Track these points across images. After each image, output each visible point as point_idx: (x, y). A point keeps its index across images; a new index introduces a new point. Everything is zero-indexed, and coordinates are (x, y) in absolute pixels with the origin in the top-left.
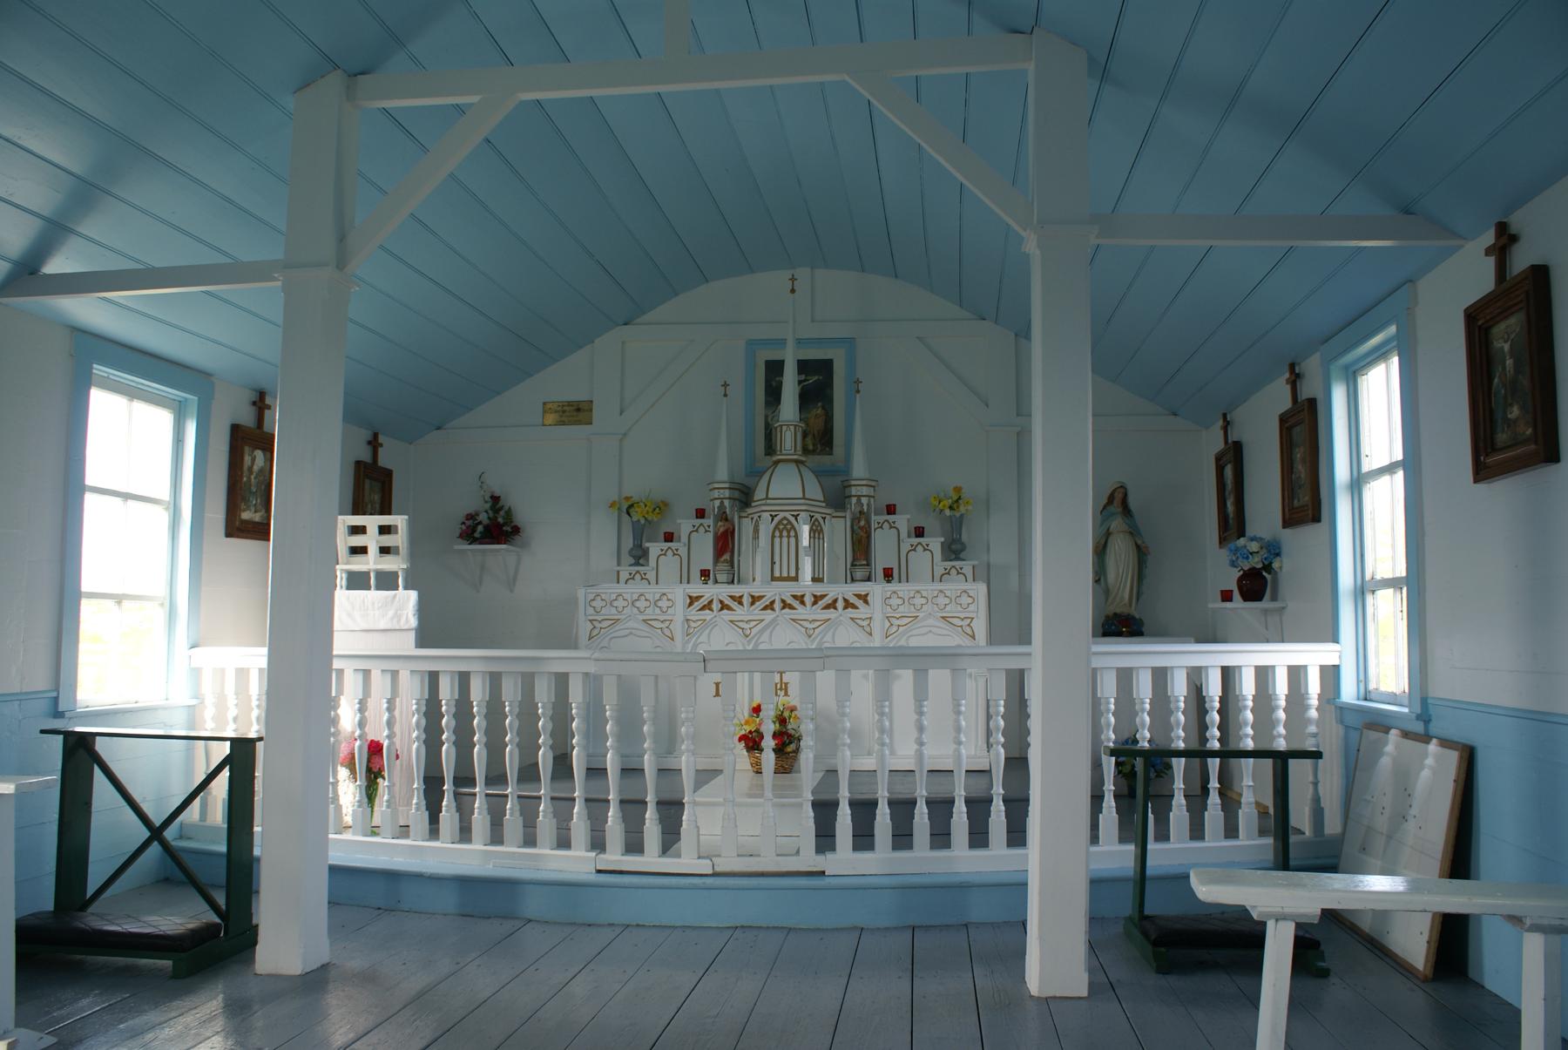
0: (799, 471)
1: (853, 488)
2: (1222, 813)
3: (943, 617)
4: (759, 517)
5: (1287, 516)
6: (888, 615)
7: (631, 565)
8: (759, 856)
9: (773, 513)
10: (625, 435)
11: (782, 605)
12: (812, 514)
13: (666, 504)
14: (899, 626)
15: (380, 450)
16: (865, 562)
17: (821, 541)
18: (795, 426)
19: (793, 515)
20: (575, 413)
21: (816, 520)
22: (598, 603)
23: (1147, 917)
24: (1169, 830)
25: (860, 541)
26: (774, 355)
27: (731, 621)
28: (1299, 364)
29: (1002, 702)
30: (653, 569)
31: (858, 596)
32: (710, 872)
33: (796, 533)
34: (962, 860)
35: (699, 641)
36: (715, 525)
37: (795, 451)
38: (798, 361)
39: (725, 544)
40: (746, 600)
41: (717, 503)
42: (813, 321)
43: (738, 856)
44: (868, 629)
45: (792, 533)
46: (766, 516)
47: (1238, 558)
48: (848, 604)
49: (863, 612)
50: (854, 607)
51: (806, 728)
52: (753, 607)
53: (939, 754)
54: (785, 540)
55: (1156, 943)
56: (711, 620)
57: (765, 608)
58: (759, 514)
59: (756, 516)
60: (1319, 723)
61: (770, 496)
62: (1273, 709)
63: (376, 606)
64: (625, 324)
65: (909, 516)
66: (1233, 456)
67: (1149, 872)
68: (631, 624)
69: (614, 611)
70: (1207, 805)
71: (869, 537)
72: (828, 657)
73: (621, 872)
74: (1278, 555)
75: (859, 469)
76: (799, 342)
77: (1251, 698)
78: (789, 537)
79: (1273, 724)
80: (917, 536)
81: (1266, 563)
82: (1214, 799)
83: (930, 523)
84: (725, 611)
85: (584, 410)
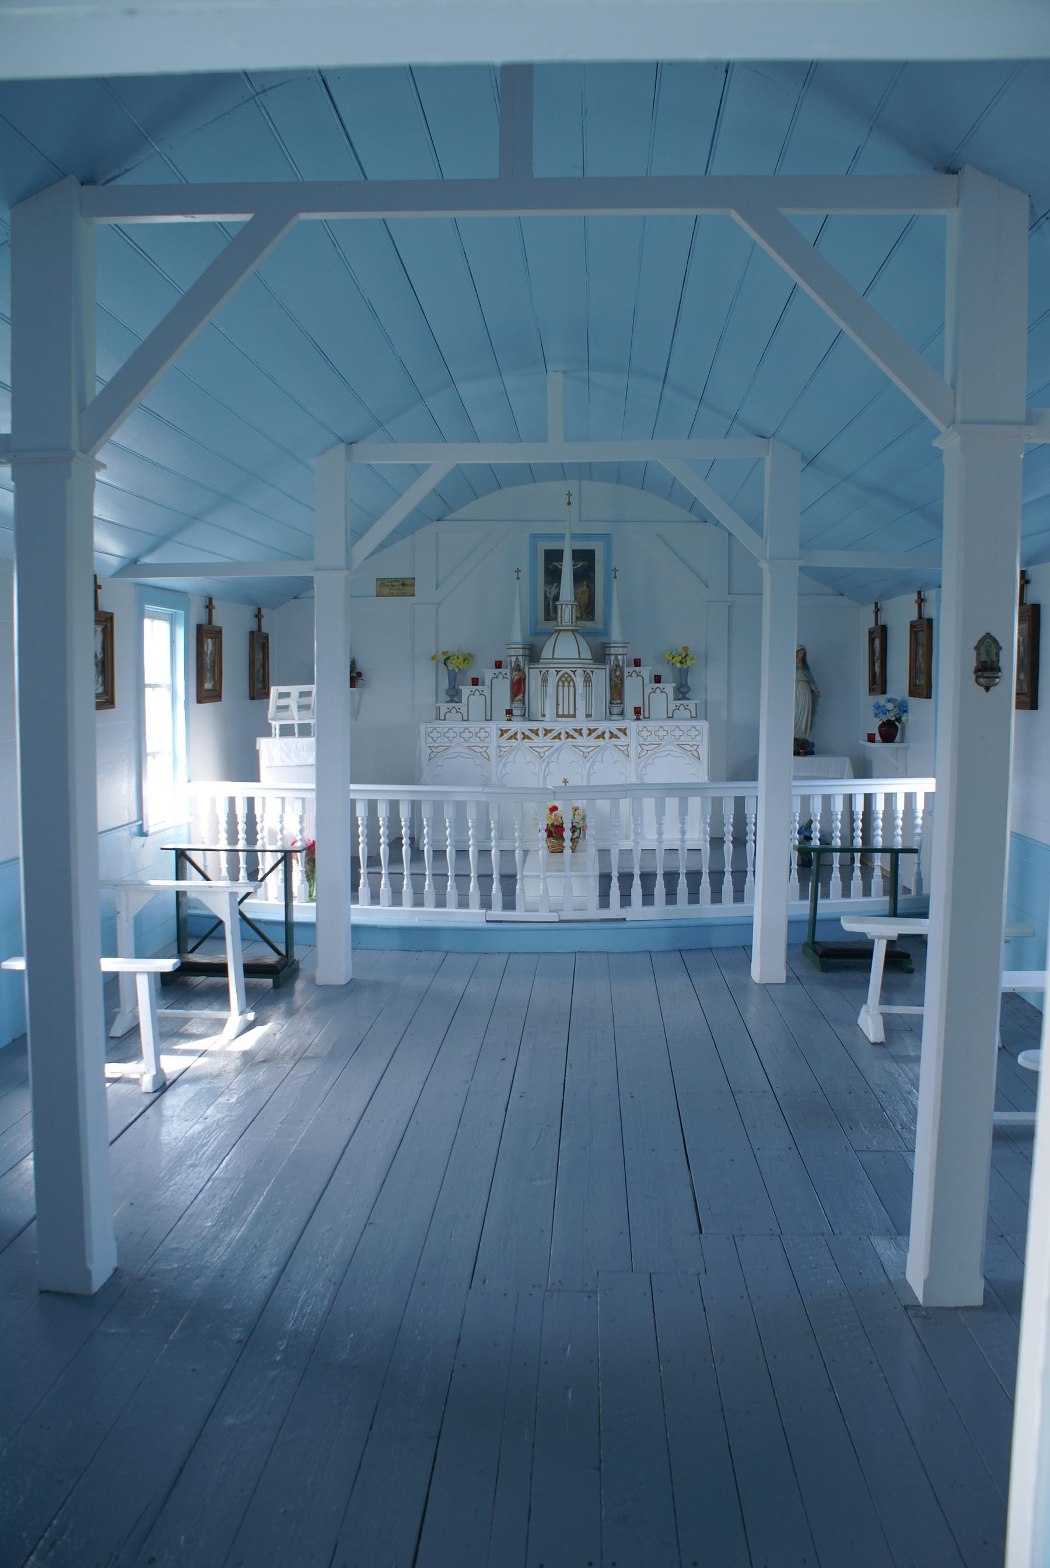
0: (575, 637)
1: (612, 649)
2: (862, 882)
3: (678, 745)
4: (547, 671)
5: (912, 690)
6: (641, 743)
7: (447, 702)
8: (586, 910)
9: (558, 670)
10: (439, 604)
11: (566, 735)
12: (585, 670)
13: (471, 656)
14: (648, 750)
15: (262, 619)
16: (619, 701)
17: (590, 688)
18: (572, 605)
19: (572, 671)
20: (401, 587)
21: (588, 673)
22: (434, 735)
23: (816, 943)
24: (829, 890)
25: (616, 686)
26: (554, 546)
27: (530, 747)
28: (924, 591)
29: (732, 816)
30: (465, 705)
31: (620, 730)
32: (558, 920)
33: (574, 683)
34: (706, 910)
35: (507, 761)
36: (512, 674)
37: (572, 622)
38: (573, 551)
39: (518, 688)
40: (541, 732)
41: (514, 659)
42: (580, 521)
43: (574, 910)
44: (626, 753)
45: (571, 684)
46: (553, 671)
47: (879, 713)
48: (612, 736)
49: (623, 740)
50: (617, 737)
51: (590, 822)
52: (546, 737)
53: (672, 837)
54: (566, 688)
55: (821, 956)
56: (516, 746)
57: (554, 738)
58: (547, 670)
59: (544, 670)
60: (922, 827)
61: (555, 657)
62: (895, 819)
63: (305, 749)
64: (438, 520)
65: (651, 668)
66: (880, 634)
67: (818, 917)
68: (459, 749)
69: (446, 740)
70: (852, 877)
71: (622, 683)
72: (628, 790)
73: (501, 922)
74: (906, 711)
75: (616, 634)
76: (575, 537)
77: (881, 812)
78: (569, 686)
79: (895, 828)
80: (656, 682)
81: (898, 717)
82: (857, 873)
83: (665, 672)
84: (526, 740)
85: (408, 585)
